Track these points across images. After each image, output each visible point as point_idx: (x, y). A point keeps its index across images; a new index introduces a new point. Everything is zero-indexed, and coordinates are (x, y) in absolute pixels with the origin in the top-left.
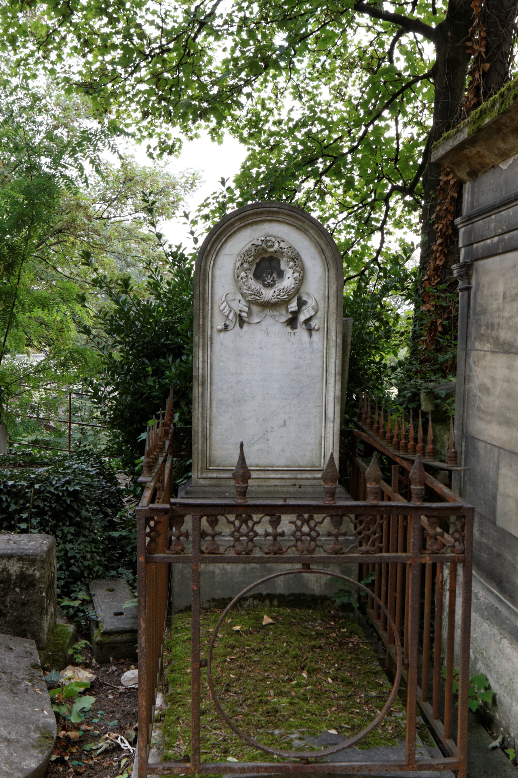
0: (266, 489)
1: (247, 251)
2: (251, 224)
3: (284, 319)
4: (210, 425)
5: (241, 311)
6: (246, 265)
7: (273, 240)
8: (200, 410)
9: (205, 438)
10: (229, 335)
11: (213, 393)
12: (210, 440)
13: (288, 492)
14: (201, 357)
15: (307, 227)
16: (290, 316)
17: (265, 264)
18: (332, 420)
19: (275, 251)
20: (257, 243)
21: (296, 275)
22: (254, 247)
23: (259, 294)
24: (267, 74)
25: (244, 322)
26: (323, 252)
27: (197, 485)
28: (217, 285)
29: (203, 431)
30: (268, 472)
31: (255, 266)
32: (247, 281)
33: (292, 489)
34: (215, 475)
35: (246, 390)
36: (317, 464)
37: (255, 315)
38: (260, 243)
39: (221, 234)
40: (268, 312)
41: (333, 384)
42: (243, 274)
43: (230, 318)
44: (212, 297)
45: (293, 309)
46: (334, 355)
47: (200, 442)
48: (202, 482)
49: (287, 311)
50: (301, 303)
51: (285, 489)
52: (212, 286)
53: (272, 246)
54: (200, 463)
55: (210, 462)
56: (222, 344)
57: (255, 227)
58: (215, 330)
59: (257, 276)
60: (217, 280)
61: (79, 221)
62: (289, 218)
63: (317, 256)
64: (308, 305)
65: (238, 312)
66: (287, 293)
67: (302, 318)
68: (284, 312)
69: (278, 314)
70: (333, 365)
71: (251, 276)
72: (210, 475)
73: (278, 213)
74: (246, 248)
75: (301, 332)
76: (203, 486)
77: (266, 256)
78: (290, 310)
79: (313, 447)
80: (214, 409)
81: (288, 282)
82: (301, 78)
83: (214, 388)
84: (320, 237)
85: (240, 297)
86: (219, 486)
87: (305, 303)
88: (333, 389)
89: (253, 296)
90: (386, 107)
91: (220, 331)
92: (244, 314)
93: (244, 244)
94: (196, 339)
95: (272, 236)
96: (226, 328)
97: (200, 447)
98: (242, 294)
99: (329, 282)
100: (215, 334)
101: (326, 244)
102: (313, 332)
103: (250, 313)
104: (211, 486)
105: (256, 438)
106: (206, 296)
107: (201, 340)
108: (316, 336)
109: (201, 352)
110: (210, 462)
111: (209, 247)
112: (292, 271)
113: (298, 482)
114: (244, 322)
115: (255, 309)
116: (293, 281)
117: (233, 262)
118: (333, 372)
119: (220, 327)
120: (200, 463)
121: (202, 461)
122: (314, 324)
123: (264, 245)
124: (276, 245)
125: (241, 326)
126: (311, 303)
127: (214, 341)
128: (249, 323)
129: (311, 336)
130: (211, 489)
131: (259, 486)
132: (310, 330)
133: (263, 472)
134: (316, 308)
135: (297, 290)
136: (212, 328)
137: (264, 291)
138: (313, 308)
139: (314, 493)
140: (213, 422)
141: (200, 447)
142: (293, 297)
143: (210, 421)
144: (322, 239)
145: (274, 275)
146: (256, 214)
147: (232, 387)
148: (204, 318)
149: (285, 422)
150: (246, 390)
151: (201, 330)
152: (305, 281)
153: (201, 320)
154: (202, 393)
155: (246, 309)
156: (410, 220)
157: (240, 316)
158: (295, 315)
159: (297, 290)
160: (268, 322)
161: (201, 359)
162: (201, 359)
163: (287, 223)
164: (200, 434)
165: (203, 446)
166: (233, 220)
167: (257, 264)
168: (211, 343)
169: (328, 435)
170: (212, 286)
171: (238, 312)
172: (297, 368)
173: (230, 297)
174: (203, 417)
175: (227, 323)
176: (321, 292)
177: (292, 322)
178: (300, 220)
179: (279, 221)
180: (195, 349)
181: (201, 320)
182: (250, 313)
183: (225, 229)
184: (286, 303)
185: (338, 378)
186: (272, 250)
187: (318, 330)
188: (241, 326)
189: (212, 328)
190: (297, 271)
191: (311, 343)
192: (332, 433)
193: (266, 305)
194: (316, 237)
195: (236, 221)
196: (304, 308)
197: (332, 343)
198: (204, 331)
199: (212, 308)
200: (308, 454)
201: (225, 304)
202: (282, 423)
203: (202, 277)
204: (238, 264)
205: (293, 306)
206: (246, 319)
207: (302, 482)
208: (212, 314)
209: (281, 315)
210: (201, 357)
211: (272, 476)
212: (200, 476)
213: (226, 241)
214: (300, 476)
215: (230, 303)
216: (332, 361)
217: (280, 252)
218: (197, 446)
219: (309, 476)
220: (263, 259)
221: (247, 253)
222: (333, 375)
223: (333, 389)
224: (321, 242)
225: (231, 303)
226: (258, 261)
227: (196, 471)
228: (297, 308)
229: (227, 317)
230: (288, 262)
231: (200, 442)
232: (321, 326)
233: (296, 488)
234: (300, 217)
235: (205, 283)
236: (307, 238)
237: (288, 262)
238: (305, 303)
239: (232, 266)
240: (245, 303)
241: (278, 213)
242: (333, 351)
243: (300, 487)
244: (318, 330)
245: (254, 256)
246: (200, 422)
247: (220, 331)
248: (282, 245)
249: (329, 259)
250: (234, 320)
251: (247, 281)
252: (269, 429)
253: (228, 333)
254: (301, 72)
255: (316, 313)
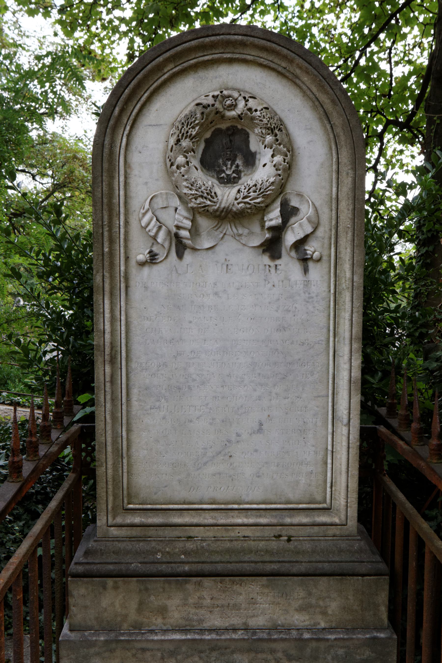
0: (228, 545)
1: (187, 118)
2: (195, 67)
3: (257, 242)
4: (129, 431)
5: (178, 227)
6: (185, 143)
7: (236, 95)
8: (108, 405)
9: (118, 454)
10: (158, 272)
11: (132, 376)
12: (129, 457)
13: (267, 551)
14: (107, 311)
15: (298, 71)
16: (268, 235)
17: (221, 140)
18: (345, 421)
19: (240, 117)
20: (205, 102)
21: (278, 159)
22: (200, 107)
23: (211, 195)
24: (255, 10)
25: (185, 247)
26: (326, 116)
27: (106, 538)
28: (134, 181)
29: (115, 442)
30: (231, 513)
31: (202, 146)
32: (187, 171)
33: (274, 545)
34: (137, 520)
35: (192, 370)
36: (319, 498)
37: (204, 234)
38: (210, 101)
39: (138, 86)
40: (228, 229)
41: (346, 357)
42: (181, 159)
43: (159, 240)
44: (126, 203)
45: (273, 223)
46: (348, 306)
47: (110, 463)
48: (114, 531)
49: (263, 226)
50: (288, 212)
51: (262, 544)
52: (126, 184)
53: (233, 106)
54: (111, 498)
55: (129, 495)
56: (146, 288)
57: (202, 73)
58: (133, 263)
59: (208, 164)
60: (135, 171)
61: (77, 173)
62: (264, 55)
63: (316, 125)
64: (301, 215)
65: (174, 230)
66: (263, 193)
67: (290, 238)
68: (256, 228)
69: (246, 231)
70: (347, 323)
71: (195, 162)
72: (129, 519)
73: (243, 44)
74: (187, 112)
75: (289, 264)
76: (117, 539)
77: (224, 126)
78: (268, 224)
79: (312, 468)
80: (135, 403)
81: (263, 173)
82: (290, 17)
83: (133, 365)
84: (321, 88)
85: (176, 202)
86: (143, 539)
87: (295, 211)
88: (348, 366)
89: (200, 200)
90: (381, 31)
91: (142, 264)
92: (184, 233)
93: (183, 105)
94: (98, 279)
95: (234, 89)
96: (153, 258)
97: (110, 472)
98: (180, 197)
99: (338, 172)
100: (134, 270)
101: (333, 101)
102: (311, 265)
103: (195, 231)
104: (130, 538)
105: (210, 454)
106: (115, 201)
107: (107, 281)
108: (316, 272)
109: (107, 302)
110: (129, 495)
111: (117, 110)
112: (270, 152)
113: (285, 531)
114: (185, 247)
115: (204, 223)
116: (273, 171)
117: (163, 138)
118: (347, 335)
119: (141, 258)
120: (111, 498)
121: (115, 496)
122: (311, 248)
123: (217, 105)
124: (241, 104)
125: (180, 256)
126: (306, 211)
127: (132, 283)
128: (194, 249)
129: (306, 271)
130: (128, 546)
131: (216, 539)
132: (305, 261)
133: (223, 514)
134: (314, 219)
135: (281, 187)
136: (127, 258)
137: (219, 190)
138: (309, 220)
139: (314, 552)
140: (135, 426)
141: (110, 472)
142: (273, 201)
143: (128, 423)
144: (327, 93)
145: (239, 162)
146: (203, 48)
147: (165, 364)
148: (112, 241)
149: (261, 424)
150: (192, 370)
151: (106, 264)
152: (294, 171)
153: (106, 244)
154: (112, 376)
155: (188, 224)
156: (401, 160)
157: (177, 236)
158: (278, 232)
159: (281, 187)
160: (229, 246)
161: (107, 315)
162: (107, 315)
163: (261, 65)
164: (109, 449)
165: (115, 469)
166: (161, 59)
167: (207, 141)
168: (127, 287)
169: (337, 447)
170: (126, 184)
171: (174, 230)
172: (282, 328)
173: (159, 203)
174: (114, 418)
175: (155, 249)
176: (324, 192)
177: (272, 247)
178: (285, 57)
179: (245, 62)
180: (97, 297)
181: (106, 244)
182: (195, 231)
183: (146, 77)
184: (261, 211)
185: (357, 346)
186: (233, 113)
187: (319, 260)
188: (180, 256)
189: (127, 258)
190: (280, 152)
191: (307, 284)
192: (345, 444)
193: (225, 217)
194: (314, 89)
195: (168, 61)
196: (293, 220)
197: (345, 284)
198: (112, 265)
199: (127, 223)
200: (303, 480)
201: (149, 214)
202: (257, 427)
203: (106, 165)
204: (172, 141)
205: (274, 217)
206: (188, 242)
207: (292, 531)
208: (127, 233)
209: (251, 233)
210: (107, 311)
211: (239, 521)
212: (110, 522)
213: (149, 99)
214: (288, 520)
215: (159, 213)
216: (345, 315)
217: (248, 117)
218: (105, 470)
219: (305, 520)
220: (217, 133)
221: (188, 121)
222: (347, 341)
223: (347, 366)
224: (323, 98)
225: (160, 214)
226: (208, 135)
227: (103, 514)
228: (280, 221)
229: (155, 238)
230: (262, 136)
231: (110, 463)
232: (325, 253)
233: (282, 543)
234: (285, 51)
235: (111, 177)
236: (297, 91)
237: (262, 136)
238: (295, 211)
239: (161, 146)
240: (185, 214)
241: (243, 44)
242: (346, 297)
243: (289, 540)
244: (319, 260)
245: (201, 125)
246: (109, 427)
247: (142, 264)
248: (252, 103)
249: (339, 130)
250: (167, 245)
251: (187, 171)
252: (233, 438)
253: (156, 268)
254: (290, 10)
255: (315, 229)
